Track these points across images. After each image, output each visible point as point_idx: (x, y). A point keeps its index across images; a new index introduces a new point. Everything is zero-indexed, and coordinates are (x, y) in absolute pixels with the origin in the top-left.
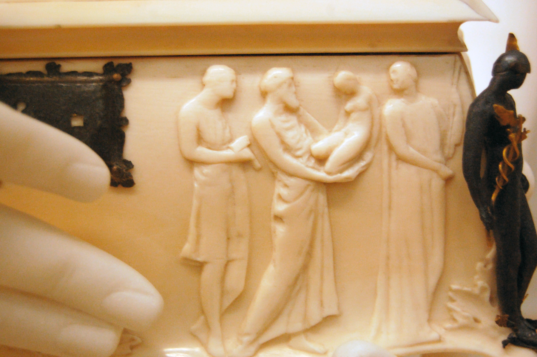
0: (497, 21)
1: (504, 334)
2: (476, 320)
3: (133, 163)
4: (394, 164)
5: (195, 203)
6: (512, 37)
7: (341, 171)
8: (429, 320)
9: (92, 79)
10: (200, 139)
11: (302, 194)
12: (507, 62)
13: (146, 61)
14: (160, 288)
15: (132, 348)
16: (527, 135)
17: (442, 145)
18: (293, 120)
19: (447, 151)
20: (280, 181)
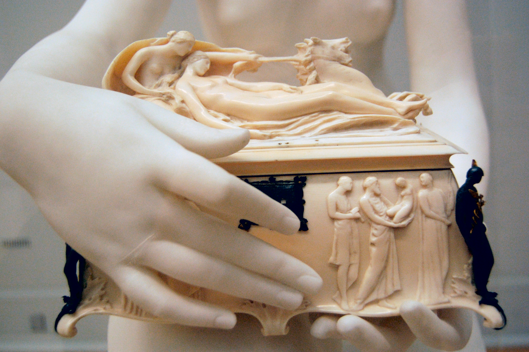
0: (467, 154)
1: (479, 298)
2: (466, 293)
3: (308, 220)
4: (424, 219)
5: (335, 238)
6: (474, 161)
7: (401, 222)
8: (444, 293)
9: (289, 183)
10: (337, 209)
11: (383, 232)
13: (313, 176)
14: (321, 276)
15: (306, 306)
17: (446, 210)
18: (378, 200)
19: (447, 213)
20: (373, 227)
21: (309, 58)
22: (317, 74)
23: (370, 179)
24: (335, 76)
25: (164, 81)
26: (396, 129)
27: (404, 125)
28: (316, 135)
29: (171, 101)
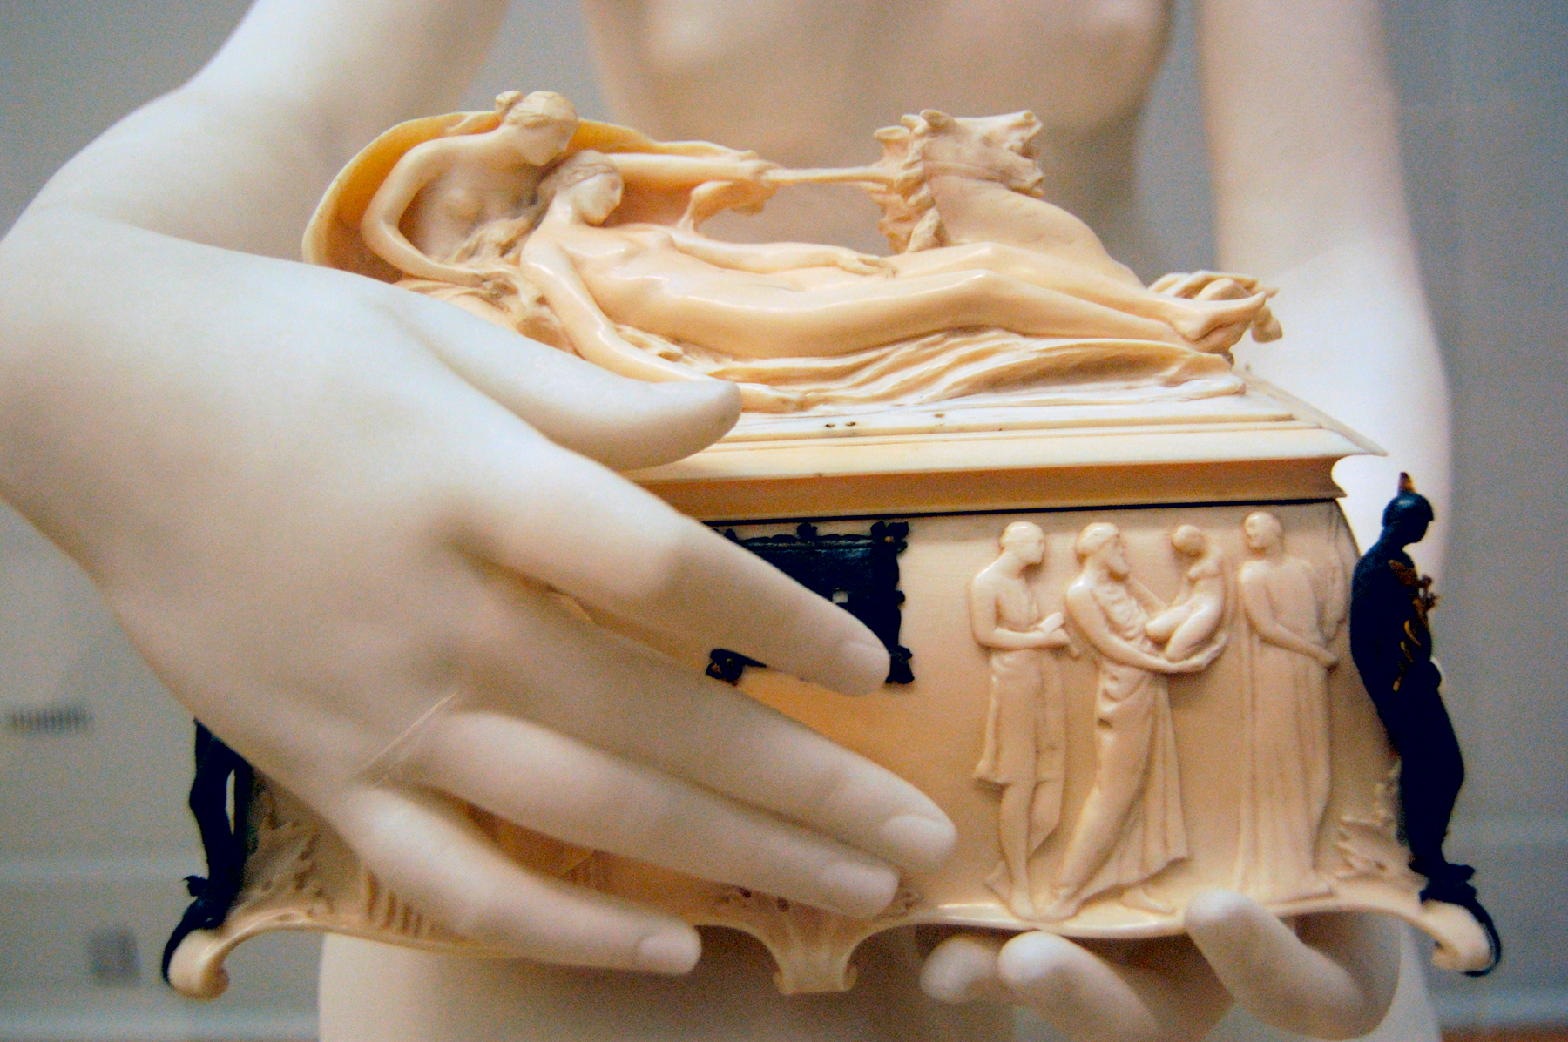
0: (1384, 455)
2: (1381, 867)
3: (912, 651)
4: (1257, 648)
5: (994, 703)
6: (1404, 476)
7: (1188, 657)
8: (1315, 867)
9: (857, 543)
10: (1000, 618)
11: (1136, 688)
12: (1401, 506)
13: (926, 520)
14: (952, 816)
15: (908, 906)
16: (1436, 602)
17: (1321, 622)
18: (1120, 591)
19: (1326, 630)
20: (1105, 672)
21: (916, 171)
22: (938, 219)
23: (1098, 531)
25: (487, 239)
26: (1172, 382)
28: (937, 399)
29: (507, 300)
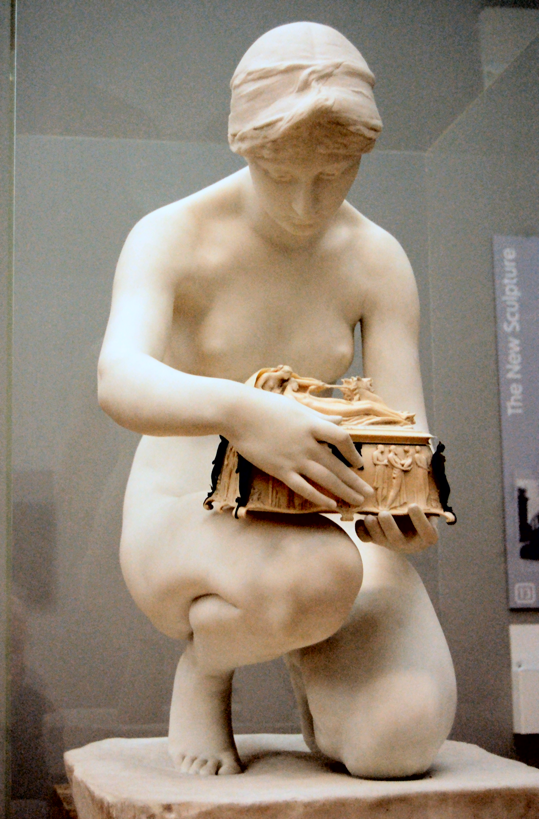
8: (427, 505)
10: (378, 460)
21: (356, 387)
23: (393, 447)
24: (368, 398)
26: (402, 426)
27: (406, 424)
